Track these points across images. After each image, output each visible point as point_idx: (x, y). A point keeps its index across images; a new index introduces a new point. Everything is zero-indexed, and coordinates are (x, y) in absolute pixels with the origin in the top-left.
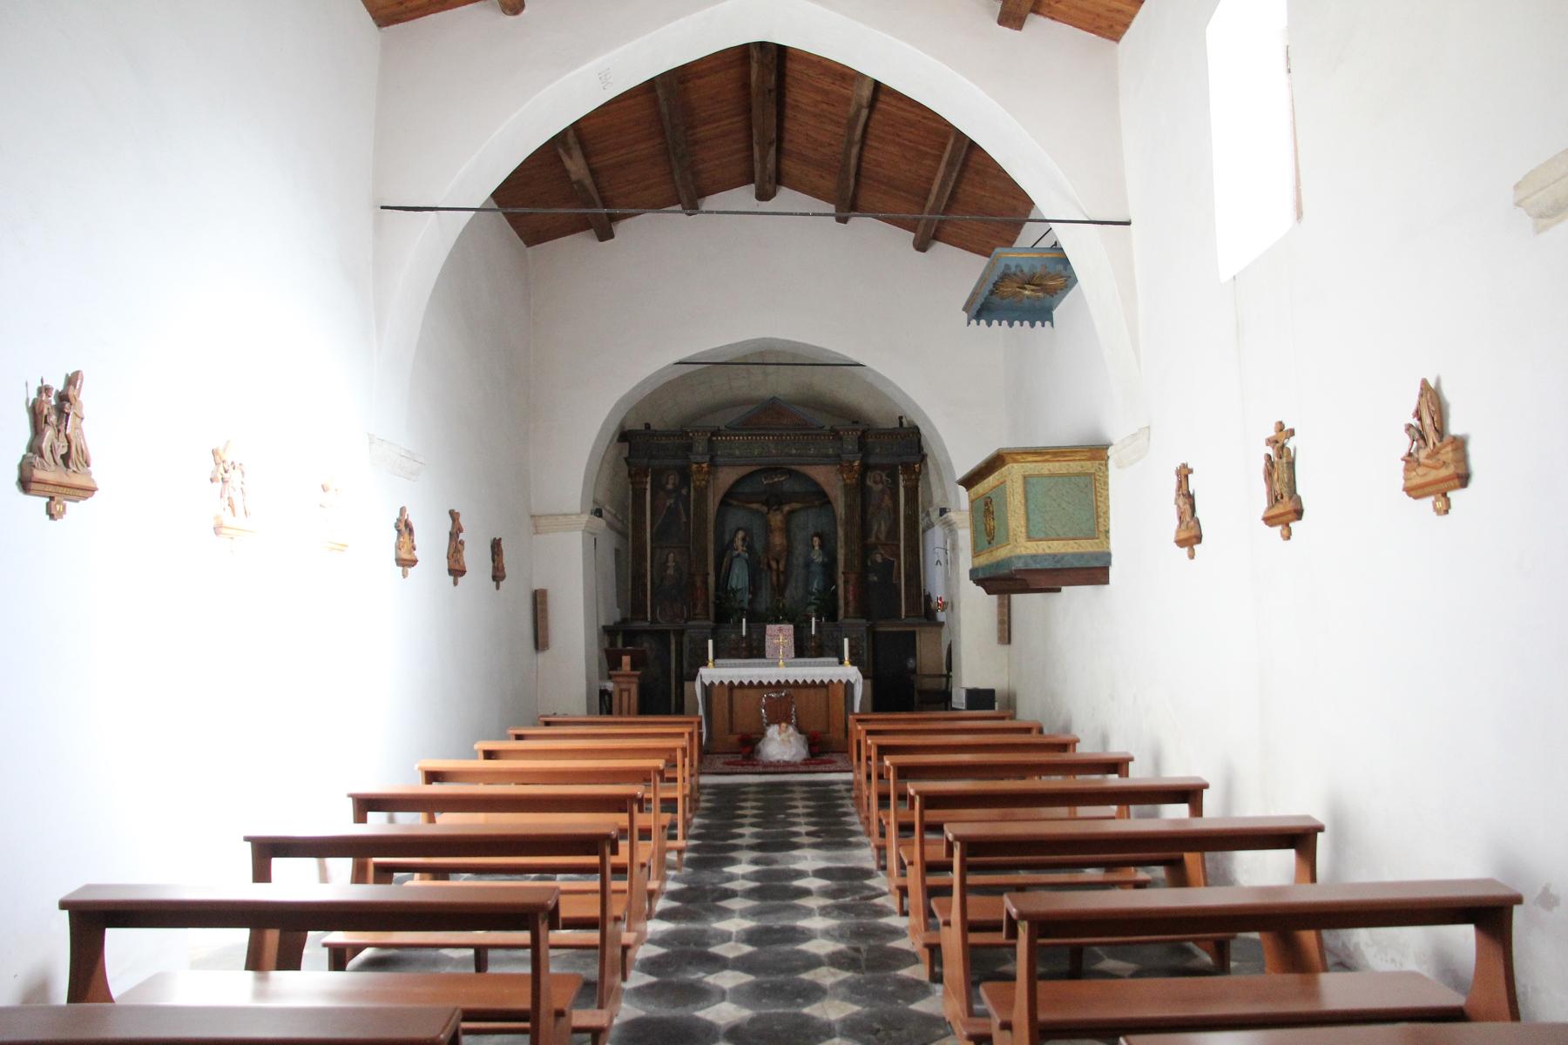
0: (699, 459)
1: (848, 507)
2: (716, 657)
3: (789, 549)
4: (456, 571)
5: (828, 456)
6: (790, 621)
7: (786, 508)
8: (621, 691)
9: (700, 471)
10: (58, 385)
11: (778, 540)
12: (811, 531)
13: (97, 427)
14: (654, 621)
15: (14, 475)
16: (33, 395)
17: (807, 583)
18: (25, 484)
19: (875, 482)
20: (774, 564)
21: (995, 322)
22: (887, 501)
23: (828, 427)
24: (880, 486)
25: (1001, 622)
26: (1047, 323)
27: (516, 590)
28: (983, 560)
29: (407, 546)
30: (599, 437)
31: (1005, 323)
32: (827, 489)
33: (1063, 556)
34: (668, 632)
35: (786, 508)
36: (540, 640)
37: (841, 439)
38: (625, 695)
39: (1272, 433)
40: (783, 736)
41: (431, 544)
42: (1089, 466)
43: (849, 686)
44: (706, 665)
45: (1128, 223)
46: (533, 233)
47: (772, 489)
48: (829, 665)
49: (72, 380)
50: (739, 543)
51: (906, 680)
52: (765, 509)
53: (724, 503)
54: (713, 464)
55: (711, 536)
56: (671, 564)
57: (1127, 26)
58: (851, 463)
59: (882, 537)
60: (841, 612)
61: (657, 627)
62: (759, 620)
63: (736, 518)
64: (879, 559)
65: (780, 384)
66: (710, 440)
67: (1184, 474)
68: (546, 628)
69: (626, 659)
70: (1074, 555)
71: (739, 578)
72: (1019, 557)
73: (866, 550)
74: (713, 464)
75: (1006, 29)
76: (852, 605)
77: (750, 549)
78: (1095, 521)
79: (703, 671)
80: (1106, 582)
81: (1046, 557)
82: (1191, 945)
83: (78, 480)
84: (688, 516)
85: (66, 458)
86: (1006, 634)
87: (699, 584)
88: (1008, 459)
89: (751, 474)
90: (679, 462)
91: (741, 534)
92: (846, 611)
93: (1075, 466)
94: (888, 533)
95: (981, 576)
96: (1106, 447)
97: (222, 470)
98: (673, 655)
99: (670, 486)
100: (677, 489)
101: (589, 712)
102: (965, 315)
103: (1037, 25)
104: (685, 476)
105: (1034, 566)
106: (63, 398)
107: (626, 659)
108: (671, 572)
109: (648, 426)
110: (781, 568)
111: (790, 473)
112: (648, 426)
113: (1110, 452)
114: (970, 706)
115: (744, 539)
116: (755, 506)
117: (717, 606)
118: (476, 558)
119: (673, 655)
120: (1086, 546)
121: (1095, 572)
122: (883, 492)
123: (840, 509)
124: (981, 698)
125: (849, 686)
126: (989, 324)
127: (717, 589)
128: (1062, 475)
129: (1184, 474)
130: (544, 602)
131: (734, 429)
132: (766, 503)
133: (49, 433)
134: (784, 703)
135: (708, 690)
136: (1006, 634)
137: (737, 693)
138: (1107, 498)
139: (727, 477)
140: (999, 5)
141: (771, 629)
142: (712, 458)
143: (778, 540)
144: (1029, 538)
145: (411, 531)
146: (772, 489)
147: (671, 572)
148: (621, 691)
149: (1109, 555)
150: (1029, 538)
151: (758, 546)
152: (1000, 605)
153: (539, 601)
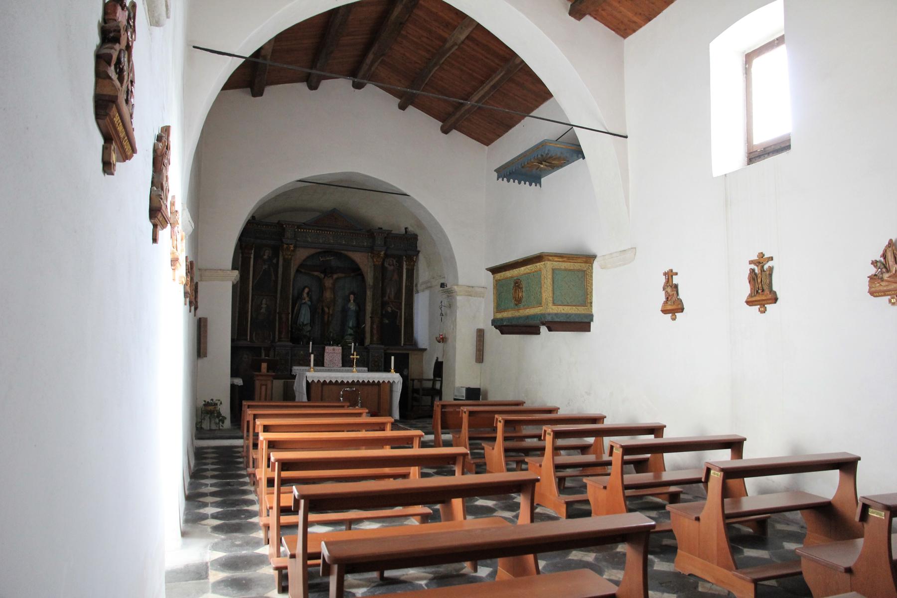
0: (289, 241)
1: (375, 278)
2: (315, 365)
9: (288, 249)
20: (326, 310)
22: (396, 276)
28: (499, 316)
32: (361, 266)
33: (571, 315)
34: (260, 348)
35: (335, 276)
38: (264, 388)
39: (755, 257)
42: (584, 266)
45: (626, 137)
47: (330, 264)
48: (364, 372)
50: (305, 295)
56: (264, 306)
57: (634, 31)
62: (321, 345)
64: (389, 309)
69: (264, 366)
70: (576, 315)
72: (549, 314)
73: (384, 304)
75: (572, 19)
78: (586, 299)
80: (589, 331)
81: (562, 315)
82: (737, 526)
84: (277, 276)
89: (319, 253)
91: (306, 290)
95: (499, 324)
96: (594, 257)
99: (266, 257)
102: (496, 174)
105: (557, 320)
107: (264, 366)
108: (263, 310)
114: (468, 398)
115: (308, 294)
116: (316, 273)
120: (581, 310)
121: (582, 324)
128: (570, 270)
129: (669, 275)
130: (206, 326)
132: (324, 272)
139: (302, 254)
140: (569, 4)
141: (328, 349)
143: (328, 295)
146: (330, 264)
147: (263, 310)
149: (592, 315)
150: (554, 304)
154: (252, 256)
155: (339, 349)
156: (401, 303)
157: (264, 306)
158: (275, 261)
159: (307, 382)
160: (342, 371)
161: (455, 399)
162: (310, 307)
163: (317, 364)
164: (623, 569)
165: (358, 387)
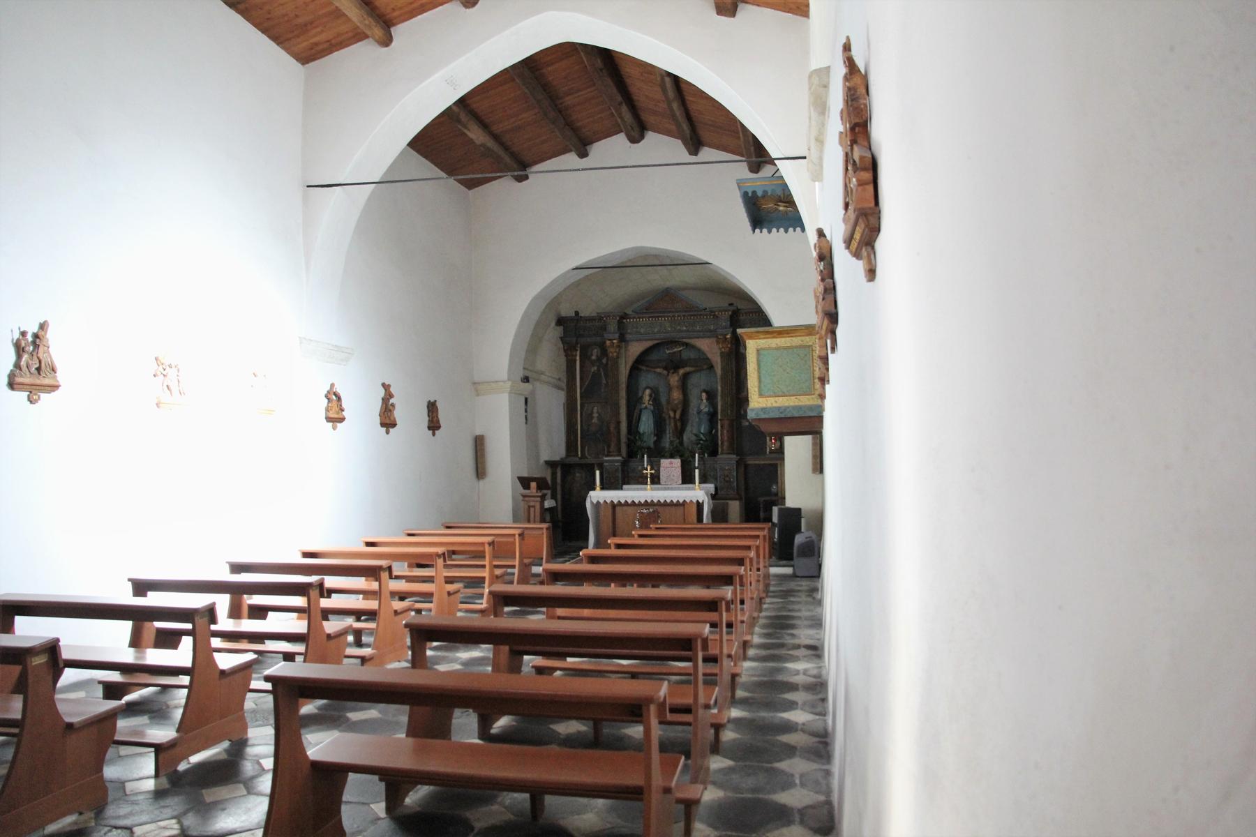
0: (611, 336)
3: (685, 403)
4: (388, 423)
10: (32, 328)
11: (677, 395)
13: (57, 349)
14: (583, 456)
15: (6, 380)
16: (17, 335)
18: (12, 385)
21: (774, 230)
25: (814, 457)
26: (798, 229)
27: (455, 433)
29: (335, 408)
31: (782, 230)
32: (709, 356)
35: (681, 371)
36: (480, 471)
41: (362, 407)
43: (700, 506)
44: (594, 489)
46: (439, 189)
47: (669, 357)
49: (43, 326)
50: (646, 398)
53: (640, 363)
54: (622, 339)
55: (623, 394)
56: (595, 415)
61: (583, 461)
62: (657, 453)
65: (658, 279)
70: (794, 408)
71: (646, 425)
74: (622, 339)
75: (723, 18)
76: (726, 444)
79: (591, 493)
81: (772, 409)
83: (47, 381)
85: (39, 369)
90: (598, 339)
91: (648, 392)
93: (796, 341)
97: (162, 368)
100: (599, 359)
103: (747, 12)
104: (604, 352)
105: (763, 416)
106: (36, 336)
108: (595, 420)
109: (577, 313)
110: (678, 416)
111: (687, 344)
112: (577, 313)
116: (658, 370)
117: (628, 446)
118: (410, 414)
120: (806, 401)
123: (719, 370)
125: (700, 506)
126: (770, 232)
131: (640, 313)
132: (665, 368)
133: (25, 357)
135: (597, 505)
137: (618, 509)
139: (635, 349)
141: (665, 462)
144: (761, 395)
145: (339, 398)
146: (669, 357)
150: (761, 395)
151: (663, 400)
152: (814, 444)
153: (479, 444)
155: (677, 462)
157: (595, 415)
163: (652, 483)
164: (640, 722)
165: (660, 509)
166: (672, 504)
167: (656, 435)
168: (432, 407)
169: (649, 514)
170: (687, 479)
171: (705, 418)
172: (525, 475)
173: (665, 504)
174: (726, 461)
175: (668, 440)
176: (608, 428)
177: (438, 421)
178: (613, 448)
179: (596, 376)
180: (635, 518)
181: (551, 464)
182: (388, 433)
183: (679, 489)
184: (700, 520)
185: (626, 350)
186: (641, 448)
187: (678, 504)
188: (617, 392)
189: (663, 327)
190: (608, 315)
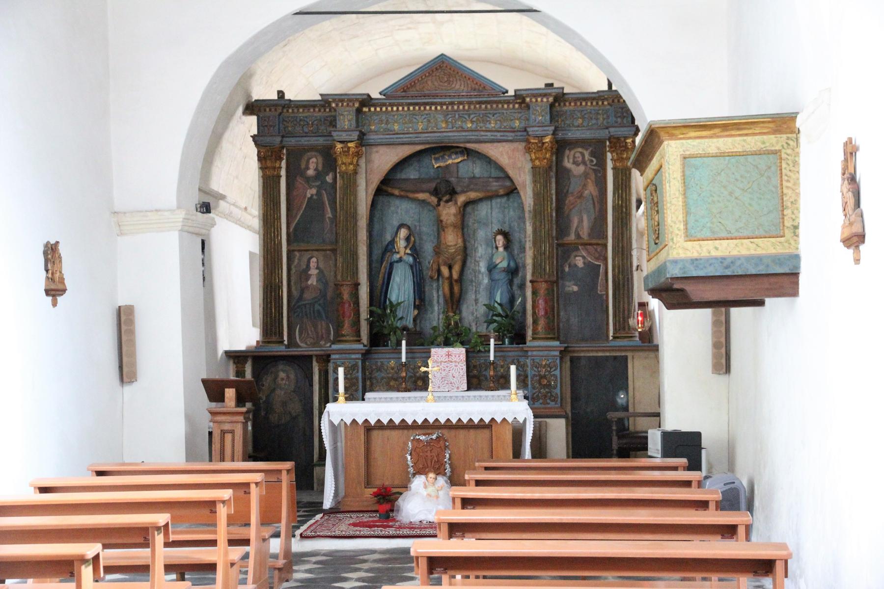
0: (344, 136)
1: (537, 196)
3: (465, 253)
5: (513, 131)
6: (463, 344)
7: (461, 199)
8: (223, 433)
9: (346, 152)
11: (452, 239)
12: (495, 229)
14: (292, 343)
17: (491, 295)
19: (575, 163)
20: (445, 271)
22: (591, 189)
23: (511, 93)
24: (582, 168)
25: (716, 345)
30: (201, 109)
33: (734, 260)
34: (309, 358)
36: (126, 371)
37: (528, 107)
38: (228, 437)
40: (431, 489)
42: (773, 141)
43: (518, 433)
44: (336, 400)
50: (401, 244)
51: (601, 421)
52: (434, 200)
53: (385, 188)
55: (363, 235)
56: (313, 272)
58: (541, 138)
59: (585, 233)
60: (529, 333)
61: (294, 351)
62: (421, 342)
63: (401, 211)
64: (580, 262)
66: (359, 111)
67: (850, 151)
68: (133, 354)
70: (749, 258)
71: (401, 289)
72: (675, 262)
76: (542, 323)
77: (416, 252)
81: (710, 261)
86: (723, 361)
87: (346, 296)
88: (662, 134)
90: (321, 141)
91: (403, 233)
92: (535, 332)
93: (751, 142)
94: (592, 229)
98: (316, 387)
99: (311, 172)
100: (319, 175)
101: (191, 455)
104: (330, 161)
108: (313, 281)
109: (281, 94)
110: (455, 276)
111: (467, 152)
112: (281, 94)
113: (799, 123)
115: (408, 239)
116: (421, 196)
117: (371, 325)
119: (316, 387)
120: (767, 247)
122: (586, 175)
123: (528, 197)
124: (686, 446)
125: (518, 433)
127: (371, 302)
129: (850, 151)
130: (131, 322)
132: (435, 192)
134: (438, 448)
136: (723, 361)
138: (797, 183)
139: (384, 159)
141: (438, 353)
142: (362, 135)
147: (313, 281)
148: (223, 433)
149: (797, 257)
150: (689, 237)
151: (428, 248)
152: (716, 323)
153: (124, 320)
154: (283, 173)
156: (605, 246)
158: (329, 179)
159: (331, 423)
160: (468, 399)
161: (44, 490)
162: (411, 266)
165: (446, 433)
166: (470, 426)
167: (416, 307)
168: (51, 253)
169: (429, 443)
170: (477, 379)
171: (502, 277)
172: (217, 376)
173: (460, 426)
174: (542, 349)
175: (436, 317)
176: (340, 295)
177: (62, 280)
178: (347, 329)
179: (315, 205)
180: (404, 449)
181: (236, 357)
182: (55, 304)
183: (463, 399)
184: (517, 453)
185: (368, 162)
186: (394, 330)
187: (482, 426)
188: (355, 235)
189: (436, 125)
190: (341, 99)
